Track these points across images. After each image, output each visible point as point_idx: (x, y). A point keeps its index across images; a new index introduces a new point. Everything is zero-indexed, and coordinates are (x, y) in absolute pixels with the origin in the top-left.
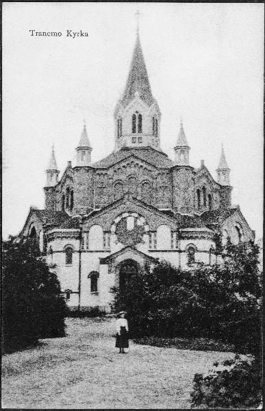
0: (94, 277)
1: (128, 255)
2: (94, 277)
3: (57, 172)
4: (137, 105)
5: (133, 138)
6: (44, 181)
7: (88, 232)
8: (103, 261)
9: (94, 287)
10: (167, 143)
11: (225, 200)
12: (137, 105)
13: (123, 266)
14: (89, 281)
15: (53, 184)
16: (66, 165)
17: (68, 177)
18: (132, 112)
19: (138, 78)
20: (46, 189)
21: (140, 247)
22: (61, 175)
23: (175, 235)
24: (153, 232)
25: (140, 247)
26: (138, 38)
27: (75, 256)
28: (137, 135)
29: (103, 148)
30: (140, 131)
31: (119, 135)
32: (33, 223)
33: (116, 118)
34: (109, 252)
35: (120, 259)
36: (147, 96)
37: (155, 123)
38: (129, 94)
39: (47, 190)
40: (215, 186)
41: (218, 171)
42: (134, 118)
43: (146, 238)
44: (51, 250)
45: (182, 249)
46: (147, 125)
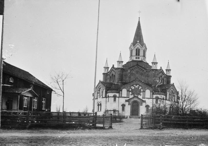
0: (123, 106)
1: (135, 99)
2: (123, 106)
3: (108, 68)
4: (138, 46)
5: (136, 57)
6: (103, 71)
7: (145, 92)
8: (126, 101)
9: (123, 109)
10: (149, 60)
11: (168, 82)
12: (138, 46)
13: (140, 33)
14: (121, 107)
15: (106, 72)
16: (112, 66)
17: (113, 70)
18: (136, 48)
19: (138, 36)
20: (104, 74)
21: (139, 97)
22: (109, 69)
23: (151, 93)
24: (144, 92)
25: (139, 97)
26: (139, 22)
27: (117, 99)
28: (138, 56)
29: (126, 59)
30: (139, 55)
31: (131, 55)
32: (100, 86)
33: (130, 49)
34: (129, 98)
35: (132, 100)
36: (142, 44)
37: (144, 52)
38: (134, 44)
39: (104, 74)
40: (165, 76)
41: (166, 70)
42: (137, 49)
43: (142, 93)
44: (108, 96)
45: (154, 98)
46: (141, 53)
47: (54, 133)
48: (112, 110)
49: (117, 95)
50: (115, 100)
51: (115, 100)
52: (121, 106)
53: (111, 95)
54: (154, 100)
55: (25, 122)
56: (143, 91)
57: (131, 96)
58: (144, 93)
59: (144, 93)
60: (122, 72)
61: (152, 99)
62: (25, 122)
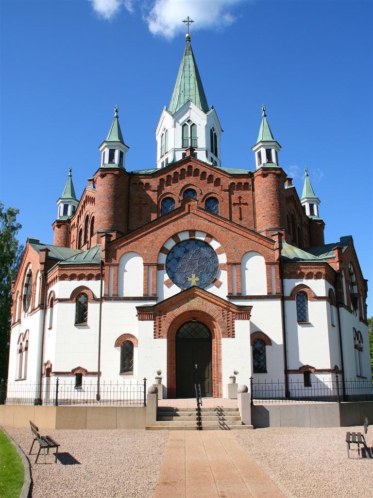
0: (127, 347)
1: (195, 304)
2: (127, 347)
14: (117, 353)
43: (223, 276)
47: (220, 380)
48: (100, 371)
49: (95, 287)
50: (81, 318)
51: (81, 318)
52: (116, 345)
53: (63, 288)
54: (287, 302)
55: (196, 366)
56: (228, 264)
57: (170, 291)
58: (235, 273)
59: (235, 273)
60: (283, 276)
61: (278, 303)
62: (196, 366)
